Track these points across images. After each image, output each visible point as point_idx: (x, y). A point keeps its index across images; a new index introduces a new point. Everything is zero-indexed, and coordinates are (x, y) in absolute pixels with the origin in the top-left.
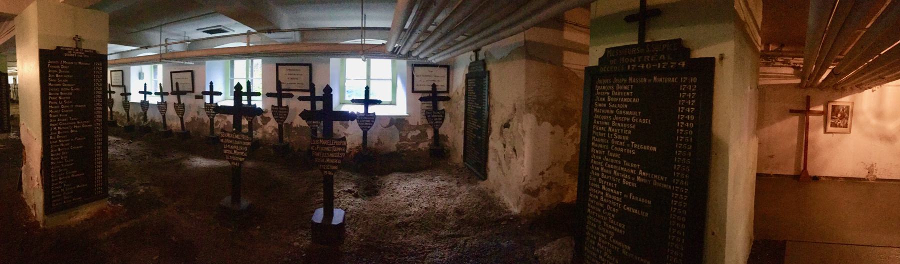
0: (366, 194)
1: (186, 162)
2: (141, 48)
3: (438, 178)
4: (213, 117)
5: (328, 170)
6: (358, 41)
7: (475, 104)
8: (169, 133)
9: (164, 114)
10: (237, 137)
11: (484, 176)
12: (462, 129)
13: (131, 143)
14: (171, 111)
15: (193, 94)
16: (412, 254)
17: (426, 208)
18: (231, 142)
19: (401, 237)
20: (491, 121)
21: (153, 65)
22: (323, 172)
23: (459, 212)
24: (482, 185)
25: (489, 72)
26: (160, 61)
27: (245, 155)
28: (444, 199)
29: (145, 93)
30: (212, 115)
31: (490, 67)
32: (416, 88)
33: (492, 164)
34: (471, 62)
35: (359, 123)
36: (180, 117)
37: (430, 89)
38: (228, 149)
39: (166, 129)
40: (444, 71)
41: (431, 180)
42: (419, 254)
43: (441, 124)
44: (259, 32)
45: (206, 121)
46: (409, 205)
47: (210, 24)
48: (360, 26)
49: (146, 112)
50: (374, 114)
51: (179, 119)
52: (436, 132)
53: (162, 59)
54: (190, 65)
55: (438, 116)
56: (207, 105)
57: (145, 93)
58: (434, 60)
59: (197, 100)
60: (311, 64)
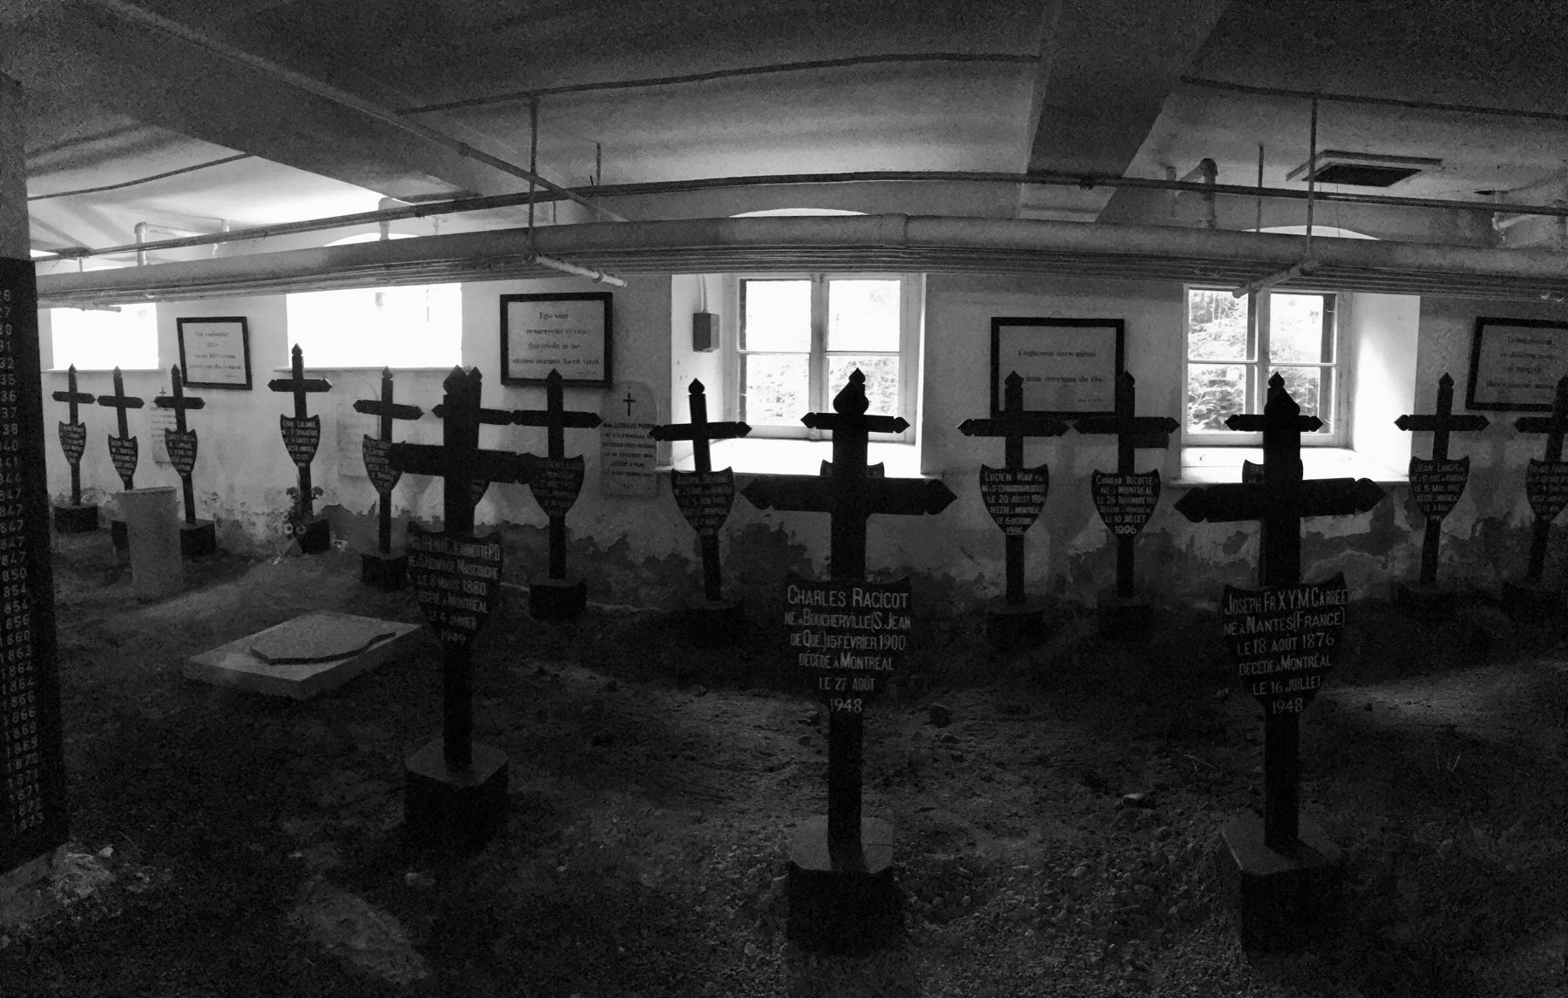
6: (1301, 230)
35: (993, 510)
49: (130, 477)
50: (729, 470)
60: (994, 320)
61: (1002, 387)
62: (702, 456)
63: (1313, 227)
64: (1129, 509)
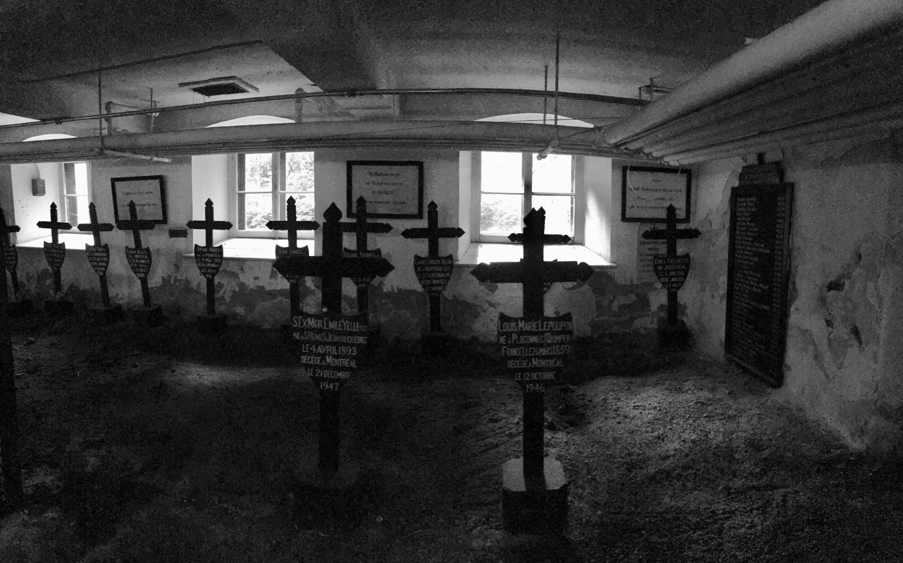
0: (567, 422)
1: (168, 377)
2: (44, 121)
3: (688, 385)
4: (213, 276)
5: (535, 382)
7: (756, 244)
8: (116, 313)
9: (104, 272)
10: (333, 325)
11: (778, 381)
12: (723, 290)
13: (32, 342)
14: (118, 265)
15: (165, 227)
16: (698, 526)
17: (693, 441)
18: (318, 337)
19: (667, 500)
20: (794, 276)
21: (63, 163)
22: (524, 388)
23: (754, 445)
24: (777, 397)
25: (792, 186)
26: (101, 154)
27: (353, 364)
28: (718, 423)
29: (54, 225)
30: (209, 271)
31: (790, 177)
32: (629, 214)
33: (794, 355)
34: (745, 164)
36: (140, 278)
37: (663, 215)
38: (310, 353)
39: (149, 306)
40: (680, 182)
41: (680, 390)
42: (709, 523)
43: (682, 283)
44: (330, 92)
45: (194, 285)
46: (659, 437)
47: (209, 73)
48: (542, 88)
51: (139, 282)
52: (673, 297)
53: (107, 149)
54: (163, 165)
55: (678, 267)
56: (199, 250)
57: (54, 225)
58: (673, 161)
59: (173, 239)
61: (354, 205)
62: (362, 242)
63: (547, 115)
64: (140, 265)
